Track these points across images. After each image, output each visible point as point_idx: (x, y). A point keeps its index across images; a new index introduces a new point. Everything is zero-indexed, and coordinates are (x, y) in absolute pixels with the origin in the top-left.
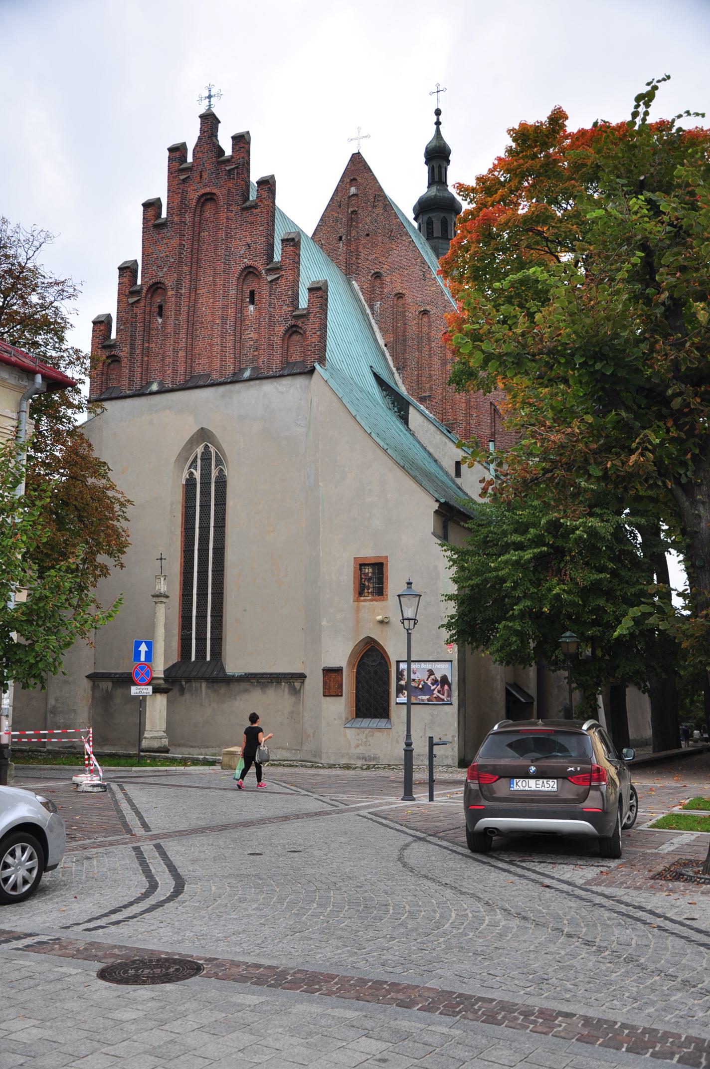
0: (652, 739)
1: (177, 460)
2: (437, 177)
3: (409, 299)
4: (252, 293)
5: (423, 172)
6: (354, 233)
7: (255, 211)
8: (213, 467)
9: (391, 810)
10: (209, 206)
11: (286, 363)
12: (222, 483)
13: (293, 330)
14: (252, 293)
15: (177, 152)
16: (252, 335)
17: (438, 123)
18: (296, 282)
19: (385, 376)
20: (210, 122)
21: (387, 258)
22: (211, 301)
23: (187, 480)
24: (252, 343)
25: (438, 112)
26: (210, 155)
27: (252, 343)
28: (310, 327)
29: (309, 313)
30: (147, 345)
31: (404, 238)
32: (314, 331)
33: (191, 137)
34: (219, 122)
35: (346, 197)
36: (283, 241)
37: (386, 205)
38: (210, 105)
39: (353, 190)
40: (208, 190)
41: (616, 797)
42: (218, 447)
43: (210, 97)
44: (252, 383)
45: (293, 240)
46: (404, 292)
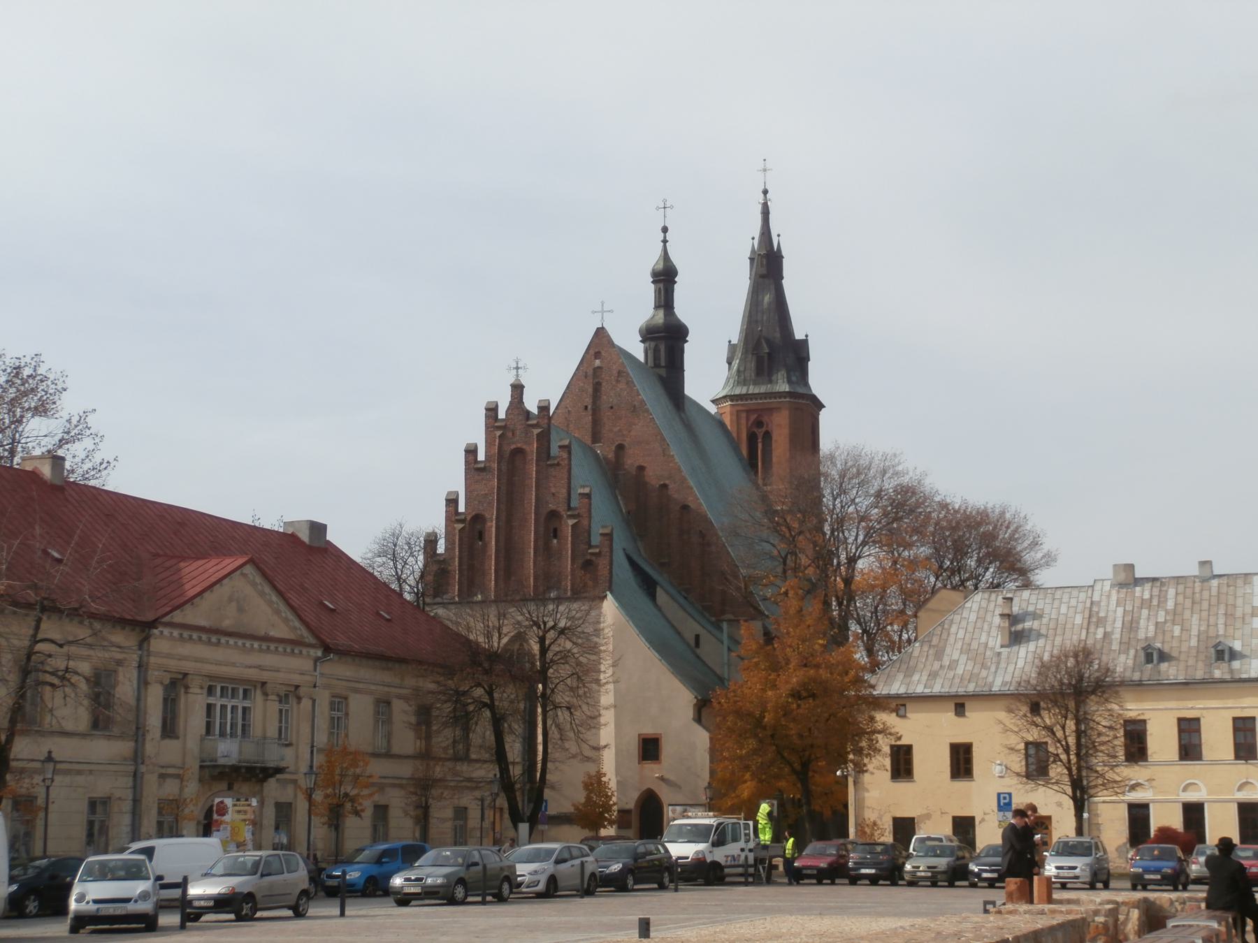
0: (810, 393)
2: (665, 299)
5: (648, 291)
15: (492, 410)
17: (665, 241)
19: (635, 557)
20: (518, 389)
25: (665, 230)
43: (517, 368)
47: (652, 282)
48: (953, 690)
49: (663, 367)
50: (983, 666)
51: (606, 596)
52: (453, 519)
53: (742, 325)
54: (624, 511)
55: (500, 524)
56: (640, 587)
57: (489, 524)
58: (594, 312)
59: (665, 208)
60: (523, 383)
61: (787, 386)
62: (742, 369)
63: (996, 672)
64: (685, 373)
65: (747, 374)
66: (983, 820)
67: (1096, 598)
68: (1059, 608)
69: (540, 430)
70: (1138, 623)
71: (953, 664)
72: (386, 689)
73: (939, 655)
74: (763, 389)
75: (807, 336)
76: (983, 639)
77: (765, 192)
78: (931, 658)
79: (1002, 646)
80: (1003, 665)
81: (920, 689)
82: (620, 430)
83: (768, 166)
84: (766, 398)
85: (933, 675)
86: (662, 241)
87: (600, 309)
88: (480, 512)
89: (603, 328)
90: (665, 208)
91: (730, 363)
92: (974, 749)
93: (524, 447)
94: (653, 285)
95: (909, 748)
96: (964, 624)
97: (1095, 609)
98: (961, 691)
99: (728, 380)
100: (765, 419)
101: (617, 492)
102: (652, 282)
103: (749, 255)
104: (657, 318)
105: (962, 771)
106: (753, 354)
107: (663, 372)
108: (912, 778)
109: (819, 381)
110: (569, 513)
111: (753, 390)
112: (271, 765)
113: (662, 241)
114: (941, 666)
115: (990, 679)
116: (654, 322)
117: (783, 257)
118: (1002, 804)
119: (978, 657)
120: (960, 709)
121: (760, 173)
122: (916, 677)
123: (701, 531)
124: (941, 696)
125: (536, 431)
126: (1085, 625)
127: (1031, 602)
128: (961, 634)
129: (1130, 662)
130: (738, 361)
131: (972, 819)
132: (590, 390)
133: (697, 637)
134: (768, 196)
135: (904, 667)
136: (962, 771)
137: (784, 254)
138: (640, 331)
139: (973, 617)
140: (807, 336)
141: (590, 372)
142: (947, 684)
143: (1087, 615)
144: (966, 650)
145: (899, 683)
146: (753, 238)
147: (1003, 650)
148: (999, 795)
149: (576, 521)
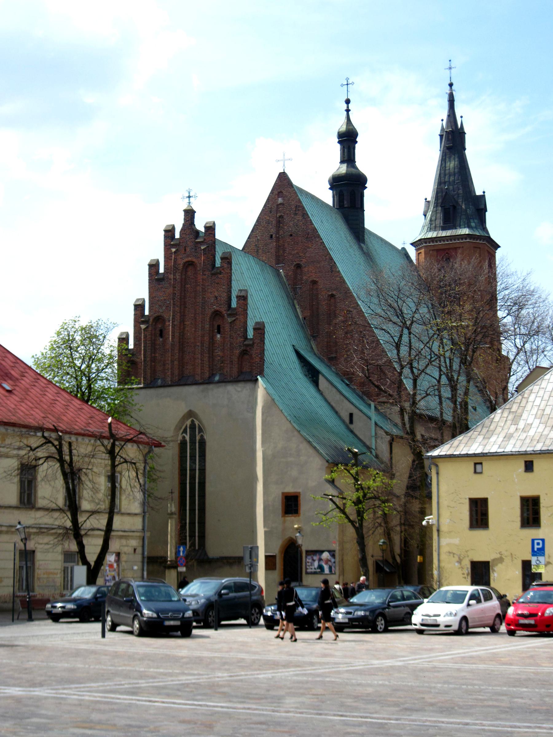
1: (175, 429)
3: (321, 286)
4: (219, 327)
5: (336, 149)
6: (281, 232)
7: (220, 276)
8: (197, 433)
10: (190, 268)
11: (241, 372)
12: (203, 443)
13: (244, 353)
14: (219, 327)
15: (169, 232)
16: (219, 353)
17: (348, 111)
18: (245, 323)
20: (190, 214)
21: (305, 254)
22: (193, 329)
23: (181, 441)
24: (219, 358)
25: (348, 102)
26: (191, 236)
27: (219, 358)
28: (254, 352)
29: (254, 343)
30: (153, 355)
31: (317, 240)
32: (257, 354)
33: (179, 225)
34: (195, 212)
35: (275, 205)
36: (237, 297)
37: (304, 213)
38: (189, 202)
39: (280, 200)
40: (190, 259)
42: (200, 421)
44: (220, 384)
45: (243, 296)
46: (317, 280)
48: (523, 449)
51: (257, 379)
53: (434, 186)
54: (301, 317)
55: (176, 323)
56: (306, 376)
57: (167, 323)
59: (347, 84)
60: (195, 209)
62: (433, 218)
64: (365, 212)
74: (448, 233)
75: (484, 192)
77: (451, 85)
78: (509, 422)
82: (297, 253)
83: (453, 66)
85: (509, 437)
87: (286, 162)
89: (284, 173)
91: (425, 215)
93: (194, 260)
96: (541, 393)
99: (423, 227)
101: (295, 302)
110: (228, 313)
111: (444, 234)
114: (517, 429)
116: (338, 173)
117: (465, 134)
118: (536, 549)
121: (447, 70)
124: (512, 455)
130: (431, 213)
133: (351, 415)
134: (453, 87)
135: (485, 430)
138: (329, 181)
140: (484, 192)
142: (519, 443)
145: (478, 444)
146: (442, 120)
148: (533, 541)
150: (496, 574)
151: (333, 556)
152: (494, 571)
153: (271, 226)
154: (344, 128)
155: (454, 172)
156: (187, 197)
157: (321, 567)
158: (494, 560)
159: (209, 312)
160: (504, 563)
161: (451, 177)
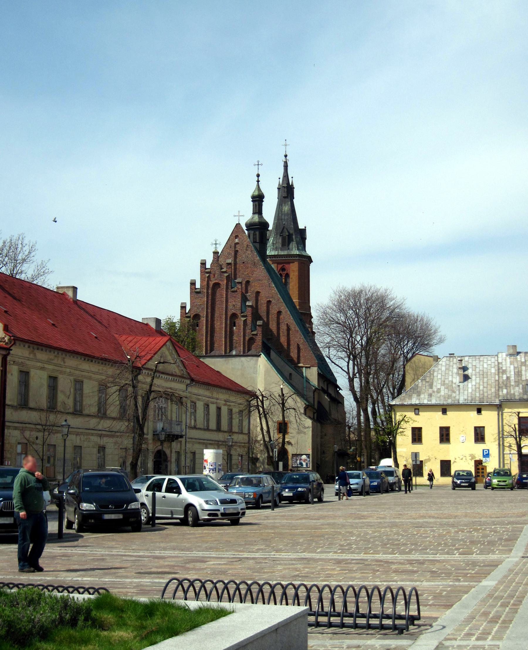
9: (267, 514)
15: (203, 264)
17: (258, 181)
21: (252, 275)
25: (258, 176)
26: (218, 268)
40: (217, 281)
41: (300, 564)
43: (216, 244)
47: (252, 201)
48: (442, 402)
49: (258, 243)
50: (454, 392)
51: (259, 356)
52: (184, 316)
57: (202, 319)
58: (239, 212)
61: (298, 251)
62: (275, 242)
63: (459, 394)
65: (277, 245)
66: (455, 462)
67: (500, 361)
68: (483, 365)
69: (227, 274)
70: (521, 372)
71: (439, 391)
72: (208, 399)
73: (431, 386)
74: (285, 253)
75: (305, 227)
76: (450, 379)
77: (286, 156)
79: (460, 382)
80: (461, 391)
81: (426, 402)
82: (247, 274)
83: (287, 143)
84: (287, 257)
86: (259, 181)
88: (198, 313)
89: (239, 224)
90: (258, 165)
92: (451, 429)
93: (220, 282)
94: (252, 203)
95: (420, 429)
97: (500, 366)
98: (445, 403)
100: (286, 266)
102: (252, 201)
103: (277, 186)
104: (255, 218)
105: (445, 439)
106: (280, 236)
107: (258, 245)
108: (422, 442)
109: (310, 249)
111: (282, 253)
112: (176, 433)
113: (259, 181)
115: (457, 397)
116: (253, 221)
117: (294, 188)
119: (449, 387)
120: (444, 412)
122: (422, 396)
123: (287, 324)
125: (226, 275)
126: (497, 373)
127: (469, 362)
128: (439, 376)
129: (521, 391)
130: (272, 238)
131: (449, 461)
132: (233, 254)
136: (445, 439)
137: (294, 186)
139: (444, 368)
141: (233, 245)
143: (497, 369)
144: (443, 384)
146: (279, 178)
147: (460, 384)
148: (483, 450)
149: (245, 318)
150: (426, 467)
151: (309, 457)
152: (425, 466)
153: (230, 256)
154: (256, 193)
155: (288, 213)
156: (214, 244)
157: (301, 464)
158: (425, 460)
159: (229, 314)
160: (431, 462)
161: (286, 216)
